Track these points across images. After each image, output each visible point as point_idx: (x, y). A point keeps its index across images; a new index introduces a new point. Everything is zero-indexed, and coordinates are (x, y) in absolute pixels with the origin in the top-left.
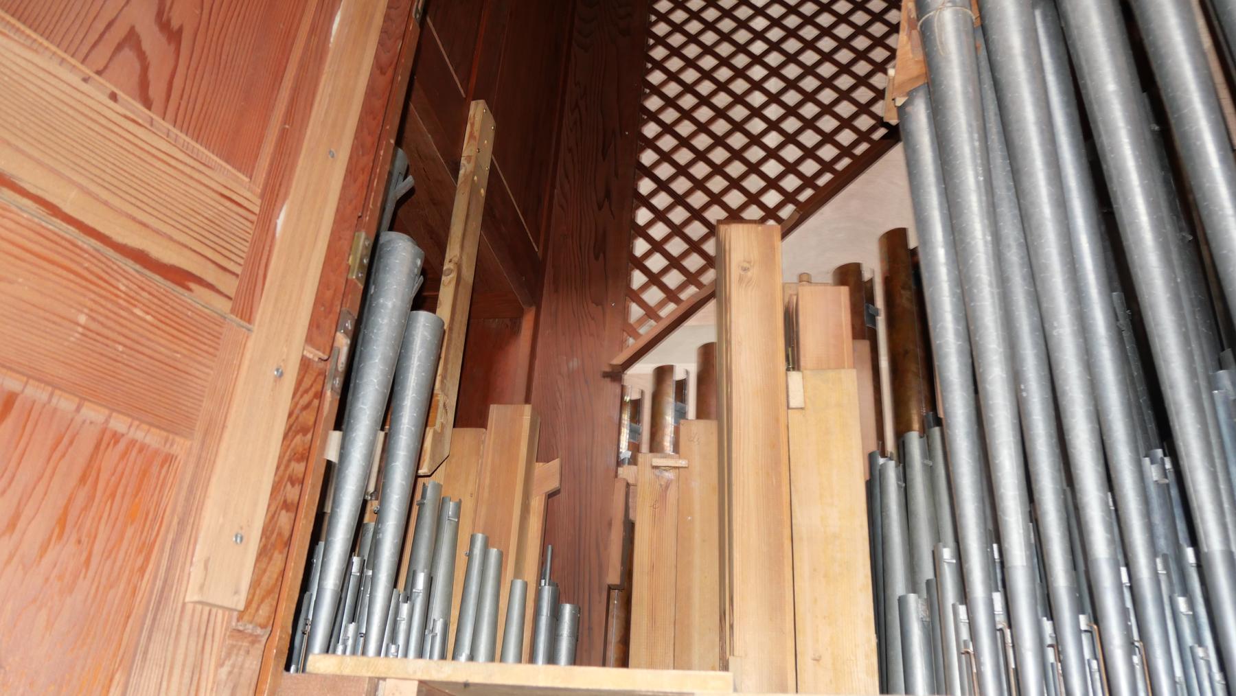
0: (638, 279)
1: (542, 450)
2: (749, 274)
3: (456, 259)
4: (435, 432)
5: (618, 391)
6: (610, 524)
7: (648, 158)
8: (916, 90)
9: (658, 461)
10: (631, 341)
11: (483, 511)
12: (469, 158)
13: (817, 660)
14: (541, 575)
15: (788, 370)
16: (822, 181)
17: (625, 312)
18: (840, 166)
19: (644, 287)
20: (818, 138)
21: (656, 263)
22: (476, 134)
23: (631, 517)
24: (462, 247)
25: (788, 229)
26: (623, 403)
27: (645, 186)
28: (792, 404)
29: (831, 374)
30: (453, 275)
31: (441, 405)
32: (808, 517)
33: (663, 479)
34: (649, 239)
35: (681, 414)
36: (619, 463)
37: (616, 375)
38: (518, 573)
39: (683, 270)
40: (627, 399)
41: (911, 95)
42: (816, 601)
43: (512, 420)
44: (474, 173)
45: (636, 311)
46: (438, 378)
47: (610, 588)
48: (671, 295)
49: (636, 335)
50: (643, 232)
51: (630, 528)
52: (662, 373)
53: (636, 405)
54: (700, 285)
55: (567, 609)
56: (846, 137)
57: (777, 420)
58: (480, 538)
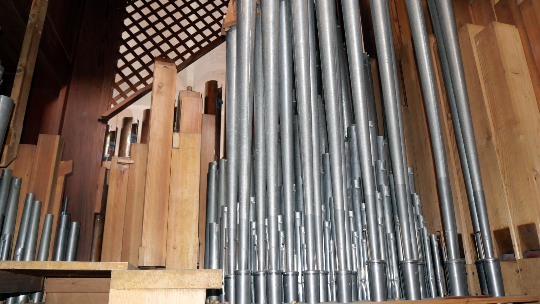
0: (118, 78)
1: (62, 156)
2: (161, 89)
3: (24, 65)
4: (9, 148)
5: (105, 128)
6: (97, 187)
7: (127, 22)
9: (121, 160)
10: (112, 106)
11: (33, 183)
12: (33, 16)
13: (175, 248)
14: (62, 210)
15: (174, 132)
16: (203, 45)
17: (111, 93)
18: (212, 40)
19: (121, 82)
20: (204, 25)
21: (127, 72)
22: (38, 4)
23: (107, 183)
24: (27, 59)
25: (179, 69)
26: (107, 133)
27: (125, 35)
28: (174, 147)
29: (191, 135)
30: (22, 73)
31: (13, 134)
32: (176, 193)
33: (124, 167)
34: (125, 60)
35: (134, 139)
36: (104, 159)
37: (104, 120)
38: (49, 211)
39: (139, 77)
40: (110, 131)
42: (176, 226)
43: (49, 142)
44: (35, 23)
45: (116, 93)
46: (12, 122)
47: (96, 214)
48: (133, 87)
49: (115, 104)
50: (122, 56)
51: (106, 188)
52: (127, 120)
53: (114, 134)
54: (146, 84)
55: (74, 224)
56: (207, 33)
57: (167, 152)
58: (31, 195)
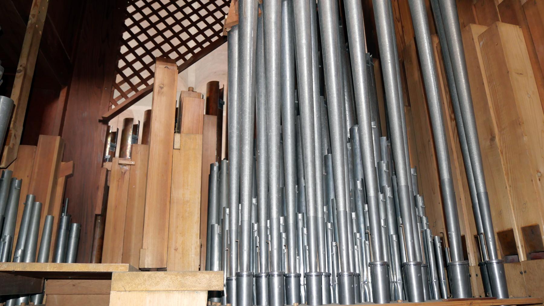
0: (119, 78)
1: (63, 157)
2: (163, 90)
3: (24, 65)
4: (9, 149)
5: (106, 129)
6: (98, 188)
7: (128, 22)
8: (235, 26)
9: (122, 161)
10: (113, 107)
11: (33, 184)
12: (34, 16)
13: (176, 250)
14: (62, 211)
15: (175, 132)
16: (205, 45)
17: (112, 93)
18: (213, 40)
19: (121, 83)
20: (205, 26)
21: (128, 72)
22: (38, 4)
23: (108, 184)
24: (28, 59)
26: (108, 134)
27: (126, 36)
28: (175, 148)
29: (192, 136)
30: (22, 73)
31: (13, 135)
32: (178, 194)
33: (125, 169)
34: (125, 61)
35: (135, 140)
36: (104, 160)
37: (105, 121)
38: (50, 212)
39: (140, 77)
40: (110, 132)
41: (233, 28)
42: (177, 227)
43: (50, 143)
44: (36, 24)
45: (116, 94)
46: (12, 123)
47: (97, 215)
48: (134, 88)
49: (116, 105)
50: (123, 57)
51: (107, 189)
52: (128, 121)
53: (115, 134)
54: (147, 85)
55: (75, 226)
57: (169, 153)
58: (31, 196)
